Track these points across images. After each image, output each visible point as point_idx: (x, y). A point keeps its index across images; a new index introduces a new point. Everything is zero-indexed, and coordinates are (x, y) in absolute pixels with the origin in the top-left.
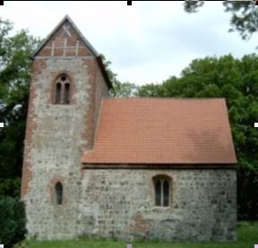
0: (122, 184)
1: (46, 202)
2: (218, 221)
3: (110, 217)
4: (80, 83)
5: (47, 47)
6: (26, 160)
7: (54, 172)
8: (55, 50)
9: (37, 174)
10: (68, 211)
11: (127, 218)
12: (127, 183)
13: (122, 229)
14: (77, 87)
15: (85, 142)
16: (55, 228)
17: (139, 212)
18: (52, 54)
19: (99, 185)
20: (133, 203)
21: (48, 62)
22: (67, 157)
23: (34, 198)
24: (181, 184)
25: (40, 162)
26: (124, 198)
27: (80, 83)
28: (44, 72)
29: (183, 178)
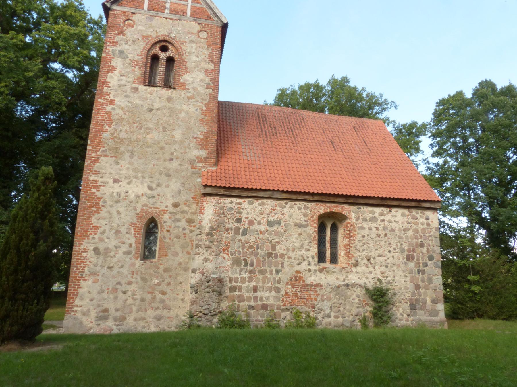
0: (270, 224)
1: (128, 253)
2: (417, 287)
3: (250, 279)
4: (194, 58)
9: (109, 203)
11: (279, 282)
12: (279, 223)
13: (271, 301)
14: (189, 65)
15: (203, 153)
16: (143, 300)
17: (298, 272)
18: (146, 7)
20: (289, 258)
21: (135, 17)
24: (363, 228)
26: (274, 247)
27: (194, 58)
28: (129, 32)
29: (365, 220)
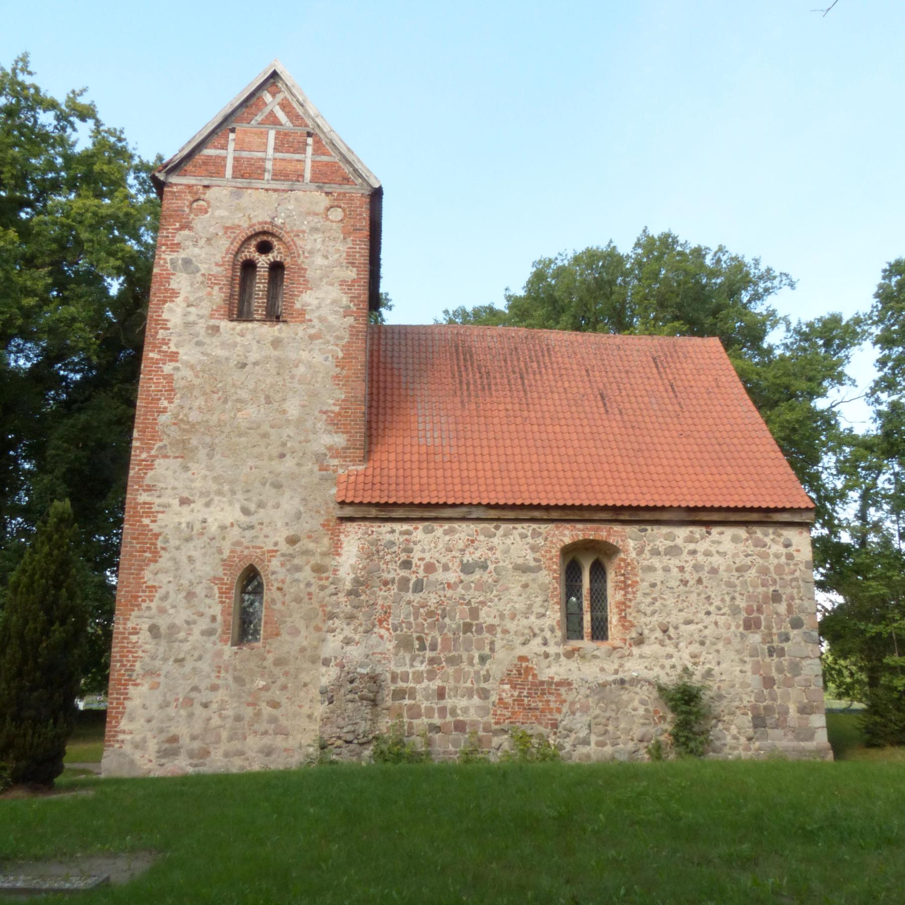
0: (467, 568)
1: (209, 633)
2: (769, 682)
3: (431, 675)
4: (319, 261)
5: (208, 152)
6: (137, 497)
7: (235, 533)
8: (236, 159)
10: (278, 662)
11: (486, 678)
12: (484, 567)
13: (472, 716)
14: (309, 274)
15: (340, 440)
16: (238, 718)
17: (522, 659)
18: (229, 172)
19: (395, 573)
20: (506, 632)
21: (210, 194)
22: (278, 486)
23: (163, 623)
24: (651, 569)
25: (184, 502)
26: (475, 613)
27: (319, 261)
29: (656, 552)
